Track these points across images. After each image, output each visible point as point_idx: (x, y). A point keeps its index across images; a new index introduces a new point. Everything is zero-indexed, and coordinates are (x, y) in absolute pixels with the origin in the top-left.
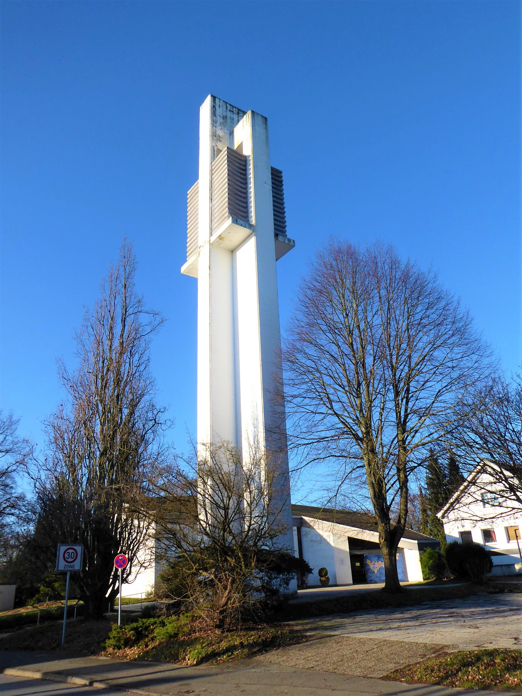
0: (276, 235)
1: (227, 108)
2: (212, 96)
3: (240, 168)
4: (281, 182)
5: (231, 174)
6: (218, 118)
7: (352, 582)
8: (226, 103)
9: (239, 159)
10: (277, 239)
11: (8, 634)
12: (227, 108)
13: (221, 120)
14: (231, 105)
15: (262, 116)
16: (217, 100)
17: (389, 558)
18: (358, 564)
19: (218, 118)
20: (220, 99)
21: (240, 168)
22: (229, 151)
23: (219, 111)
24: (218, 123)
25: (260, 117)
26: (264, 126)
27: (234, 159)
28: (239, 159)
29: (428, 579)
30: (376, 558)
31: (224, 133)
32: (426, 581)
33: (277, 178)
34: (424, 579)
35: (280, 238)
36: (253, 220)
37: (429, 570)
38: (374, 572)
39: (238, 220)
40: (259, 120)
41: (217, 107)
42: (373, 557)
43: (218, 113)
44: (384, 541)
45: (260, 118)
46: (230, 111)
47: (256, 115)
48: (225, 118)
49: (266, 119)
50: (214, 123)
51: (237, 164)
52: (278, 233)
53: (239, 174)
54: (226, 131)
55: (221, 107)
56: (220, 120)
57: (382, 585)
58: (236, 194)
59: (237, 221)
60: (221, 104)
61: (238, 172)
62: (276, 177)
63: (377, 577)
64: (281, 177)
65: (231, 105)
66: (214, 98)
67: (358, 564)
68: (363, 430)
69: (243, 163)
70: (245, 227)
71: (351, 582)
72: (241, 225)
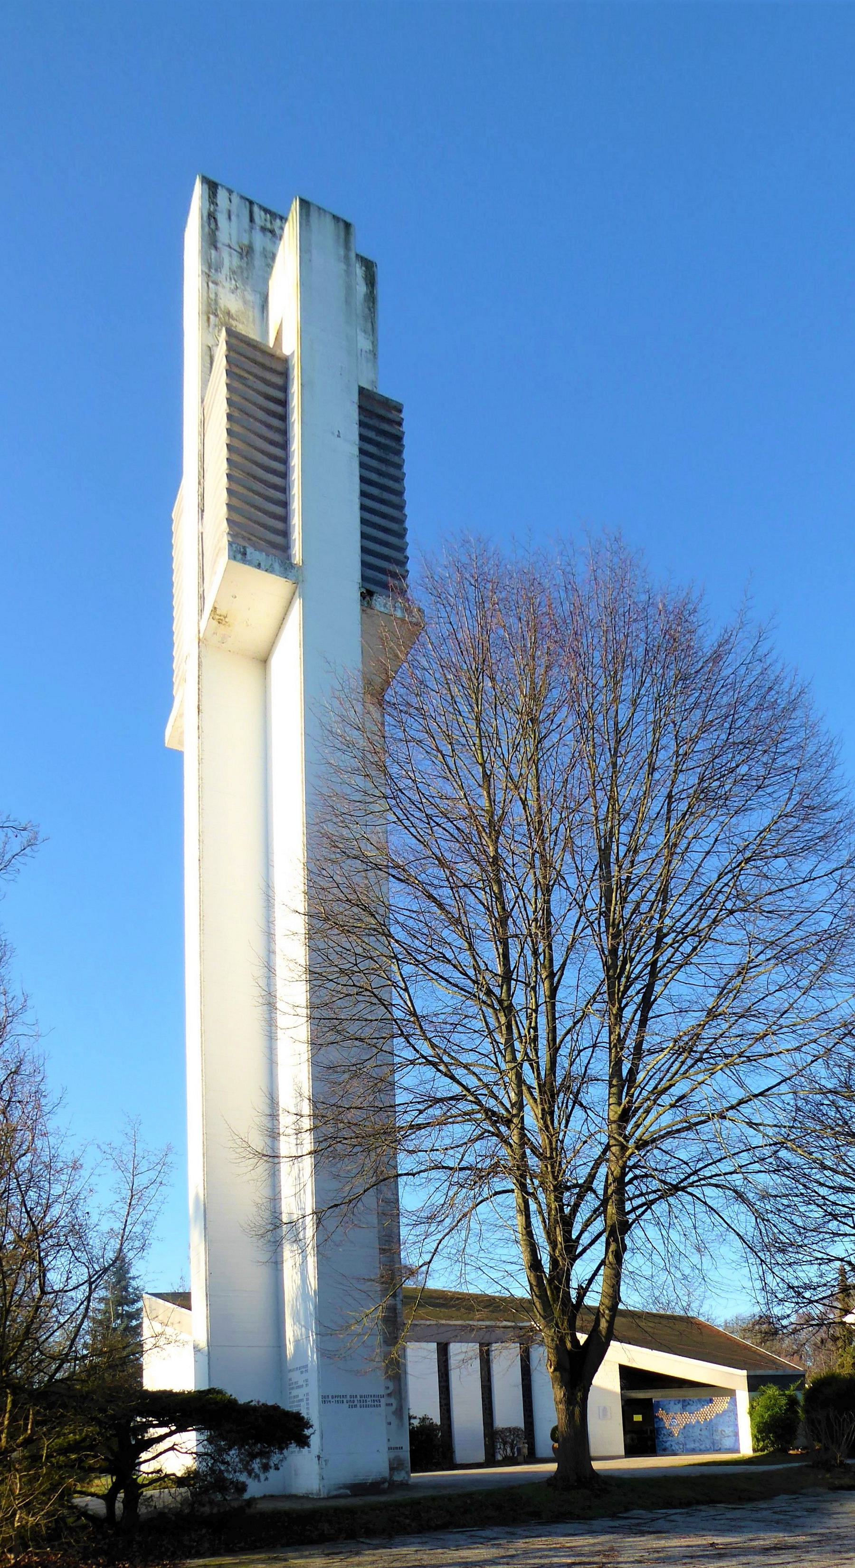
0: (367, 595)
1: (252, 220)
2: (205, 180)
3: (268, 398)
4: (398, 438)
5: (236, 414)
6: (225, 253)
7: (622, 1453)
8: (251, 203)
9: (263, 366)
10: (370, 606)
11: (797, 1465)
12: (252, 220)
13: (236, 261)
14: (266, 211)
15: (336, 219)
16: (222, 194)
17: (567, 1409)
18: (638, 1418)
19: (225, 253)
20: (230, 192)
21: (268, 398)
22: (234, 341)
23: (227, 231)
24: (225, 270)
25: (329, 220)
26: (342, 252)
27: (248, 365)
28: (263, 366)
29: (762, 1450)
30: (680, 1406)
31: (245, 302)
32: (758, 1454)
33: (386, 427)
34: (754, 1450)
35: (380, 602)
36: (297, 552)
37: (303, 1447)
38: (671, 1434)
39: (249, 550)
40: (326, 231)
41: (222, 219)
42: (672, 1403)
43: (223, 236)
44: (555, 1370)
45: (329, 223)
46: (263, 229)
47: (314, 214)
48: (246, 252)
49: (348, 226)
50: (211, 269)
51: (259, 383)
52: (372, 587)
53: (261, 415)
54: (250, 297)
55: (233, 218)
56: (229, 260)
57: (553, 1467)
58: (254, 477)
59: (245, 554)
60: (234, 210)
61: (262, 408)
62: (380, 427)
63: (678, 1443)
64: (400, 424)
65: (266, 211)
66: (212, 187)
67: (638, 1418)
68: (512, 1095)
69: (278, 380)
70: (270, 570)
71: (622, 1451)
72: (259, 566)
